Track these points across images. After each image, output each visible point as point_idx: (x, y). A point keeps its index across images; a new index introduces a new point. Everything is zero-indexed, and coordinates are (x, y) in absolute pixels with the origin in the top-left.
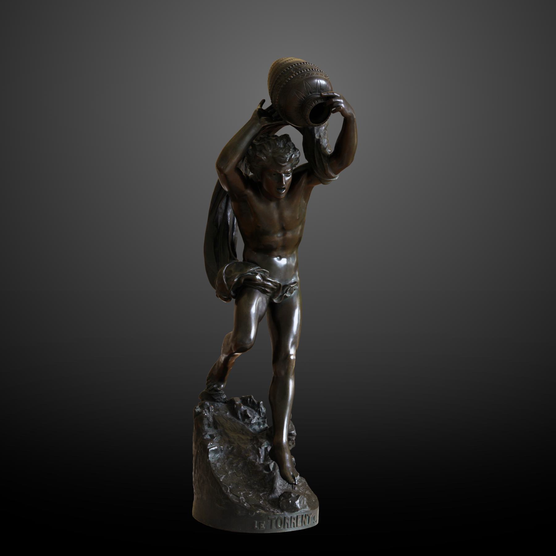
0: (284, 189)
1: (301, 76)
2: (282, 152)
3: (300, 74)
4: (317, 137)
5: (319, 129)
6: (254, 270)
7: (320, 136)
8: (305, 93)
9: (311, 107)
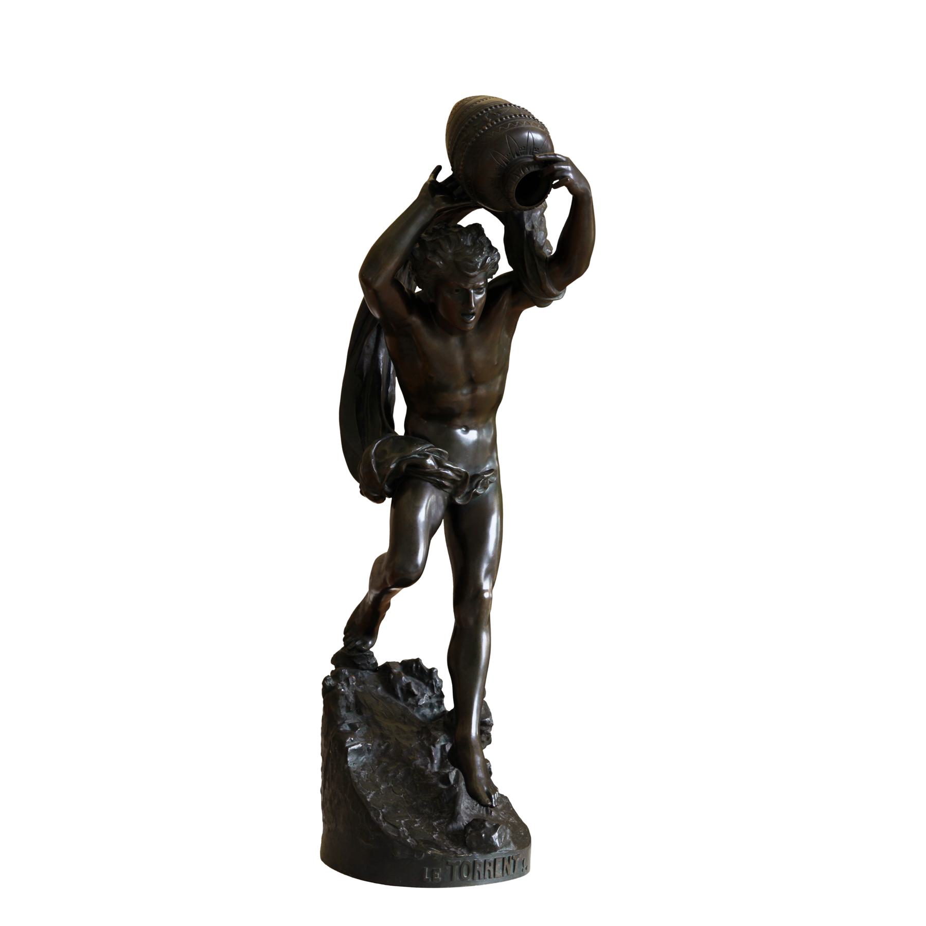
0: (473, 314)
1: (502, 126)
2: (470, 253)
3: (500, 123)
4: (528, 228)
5: (531, 215)
6: (423, 450)
7: (533, 227)
8: (507, 155)
9: (519, 179)
